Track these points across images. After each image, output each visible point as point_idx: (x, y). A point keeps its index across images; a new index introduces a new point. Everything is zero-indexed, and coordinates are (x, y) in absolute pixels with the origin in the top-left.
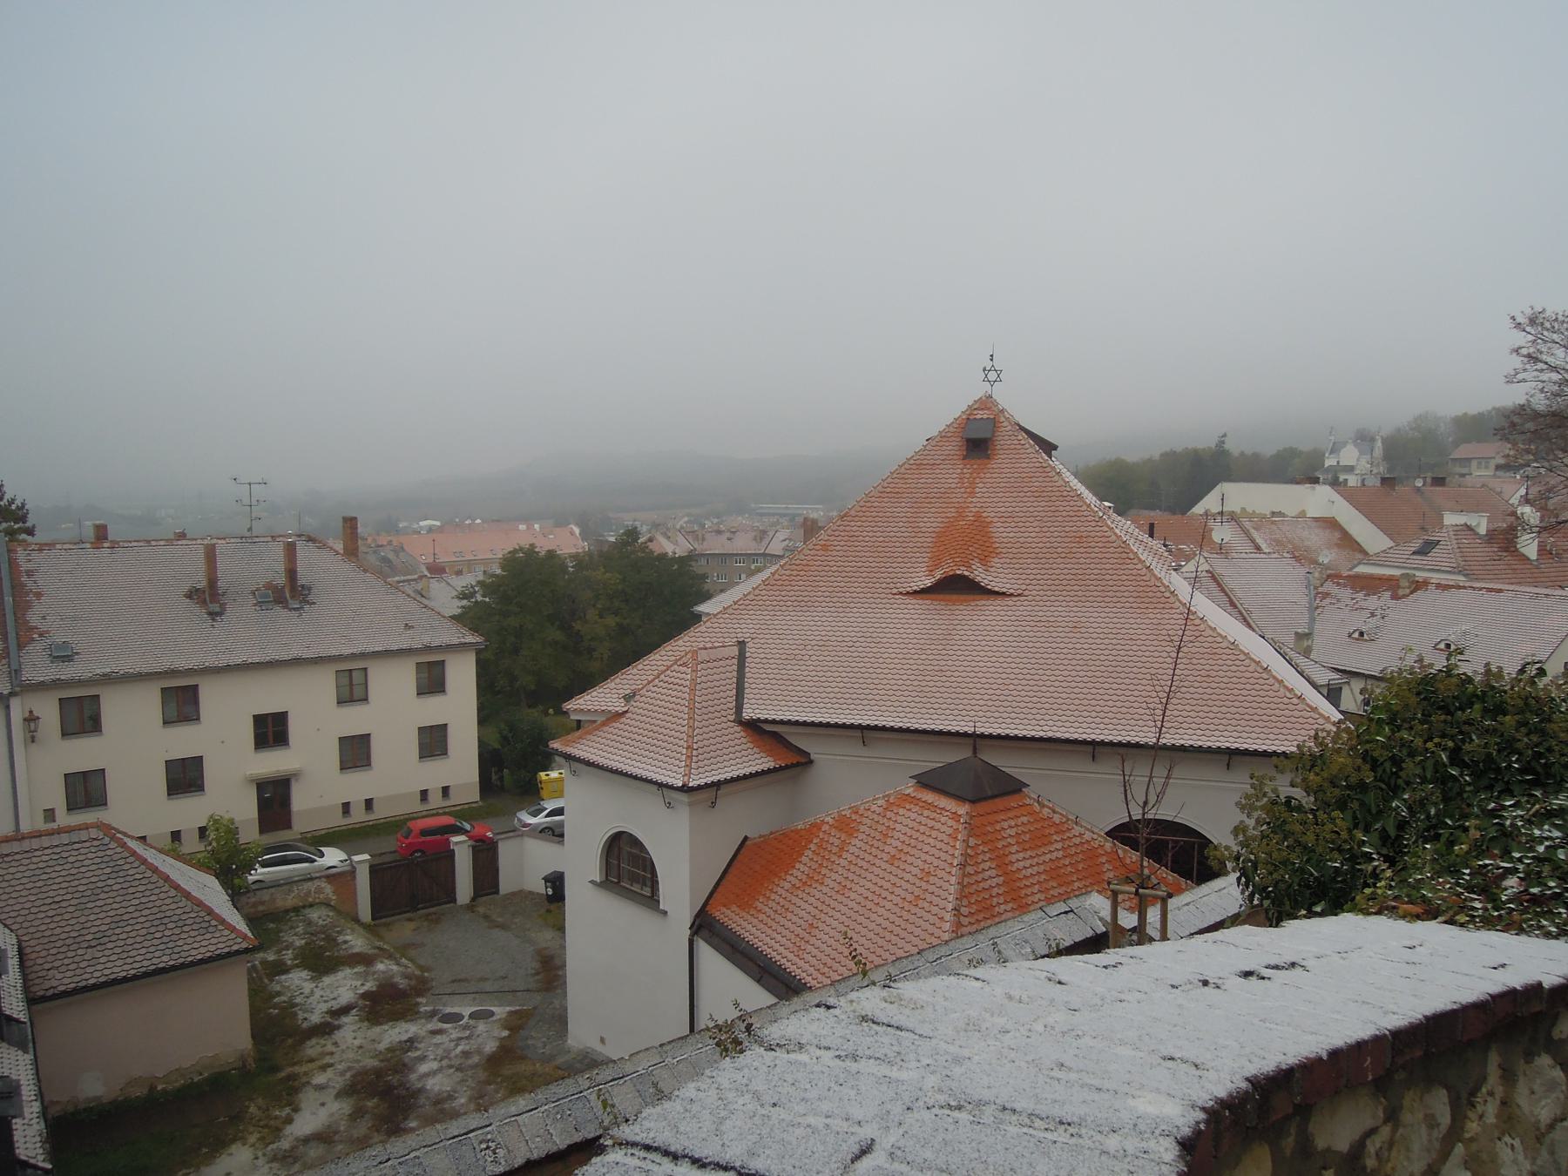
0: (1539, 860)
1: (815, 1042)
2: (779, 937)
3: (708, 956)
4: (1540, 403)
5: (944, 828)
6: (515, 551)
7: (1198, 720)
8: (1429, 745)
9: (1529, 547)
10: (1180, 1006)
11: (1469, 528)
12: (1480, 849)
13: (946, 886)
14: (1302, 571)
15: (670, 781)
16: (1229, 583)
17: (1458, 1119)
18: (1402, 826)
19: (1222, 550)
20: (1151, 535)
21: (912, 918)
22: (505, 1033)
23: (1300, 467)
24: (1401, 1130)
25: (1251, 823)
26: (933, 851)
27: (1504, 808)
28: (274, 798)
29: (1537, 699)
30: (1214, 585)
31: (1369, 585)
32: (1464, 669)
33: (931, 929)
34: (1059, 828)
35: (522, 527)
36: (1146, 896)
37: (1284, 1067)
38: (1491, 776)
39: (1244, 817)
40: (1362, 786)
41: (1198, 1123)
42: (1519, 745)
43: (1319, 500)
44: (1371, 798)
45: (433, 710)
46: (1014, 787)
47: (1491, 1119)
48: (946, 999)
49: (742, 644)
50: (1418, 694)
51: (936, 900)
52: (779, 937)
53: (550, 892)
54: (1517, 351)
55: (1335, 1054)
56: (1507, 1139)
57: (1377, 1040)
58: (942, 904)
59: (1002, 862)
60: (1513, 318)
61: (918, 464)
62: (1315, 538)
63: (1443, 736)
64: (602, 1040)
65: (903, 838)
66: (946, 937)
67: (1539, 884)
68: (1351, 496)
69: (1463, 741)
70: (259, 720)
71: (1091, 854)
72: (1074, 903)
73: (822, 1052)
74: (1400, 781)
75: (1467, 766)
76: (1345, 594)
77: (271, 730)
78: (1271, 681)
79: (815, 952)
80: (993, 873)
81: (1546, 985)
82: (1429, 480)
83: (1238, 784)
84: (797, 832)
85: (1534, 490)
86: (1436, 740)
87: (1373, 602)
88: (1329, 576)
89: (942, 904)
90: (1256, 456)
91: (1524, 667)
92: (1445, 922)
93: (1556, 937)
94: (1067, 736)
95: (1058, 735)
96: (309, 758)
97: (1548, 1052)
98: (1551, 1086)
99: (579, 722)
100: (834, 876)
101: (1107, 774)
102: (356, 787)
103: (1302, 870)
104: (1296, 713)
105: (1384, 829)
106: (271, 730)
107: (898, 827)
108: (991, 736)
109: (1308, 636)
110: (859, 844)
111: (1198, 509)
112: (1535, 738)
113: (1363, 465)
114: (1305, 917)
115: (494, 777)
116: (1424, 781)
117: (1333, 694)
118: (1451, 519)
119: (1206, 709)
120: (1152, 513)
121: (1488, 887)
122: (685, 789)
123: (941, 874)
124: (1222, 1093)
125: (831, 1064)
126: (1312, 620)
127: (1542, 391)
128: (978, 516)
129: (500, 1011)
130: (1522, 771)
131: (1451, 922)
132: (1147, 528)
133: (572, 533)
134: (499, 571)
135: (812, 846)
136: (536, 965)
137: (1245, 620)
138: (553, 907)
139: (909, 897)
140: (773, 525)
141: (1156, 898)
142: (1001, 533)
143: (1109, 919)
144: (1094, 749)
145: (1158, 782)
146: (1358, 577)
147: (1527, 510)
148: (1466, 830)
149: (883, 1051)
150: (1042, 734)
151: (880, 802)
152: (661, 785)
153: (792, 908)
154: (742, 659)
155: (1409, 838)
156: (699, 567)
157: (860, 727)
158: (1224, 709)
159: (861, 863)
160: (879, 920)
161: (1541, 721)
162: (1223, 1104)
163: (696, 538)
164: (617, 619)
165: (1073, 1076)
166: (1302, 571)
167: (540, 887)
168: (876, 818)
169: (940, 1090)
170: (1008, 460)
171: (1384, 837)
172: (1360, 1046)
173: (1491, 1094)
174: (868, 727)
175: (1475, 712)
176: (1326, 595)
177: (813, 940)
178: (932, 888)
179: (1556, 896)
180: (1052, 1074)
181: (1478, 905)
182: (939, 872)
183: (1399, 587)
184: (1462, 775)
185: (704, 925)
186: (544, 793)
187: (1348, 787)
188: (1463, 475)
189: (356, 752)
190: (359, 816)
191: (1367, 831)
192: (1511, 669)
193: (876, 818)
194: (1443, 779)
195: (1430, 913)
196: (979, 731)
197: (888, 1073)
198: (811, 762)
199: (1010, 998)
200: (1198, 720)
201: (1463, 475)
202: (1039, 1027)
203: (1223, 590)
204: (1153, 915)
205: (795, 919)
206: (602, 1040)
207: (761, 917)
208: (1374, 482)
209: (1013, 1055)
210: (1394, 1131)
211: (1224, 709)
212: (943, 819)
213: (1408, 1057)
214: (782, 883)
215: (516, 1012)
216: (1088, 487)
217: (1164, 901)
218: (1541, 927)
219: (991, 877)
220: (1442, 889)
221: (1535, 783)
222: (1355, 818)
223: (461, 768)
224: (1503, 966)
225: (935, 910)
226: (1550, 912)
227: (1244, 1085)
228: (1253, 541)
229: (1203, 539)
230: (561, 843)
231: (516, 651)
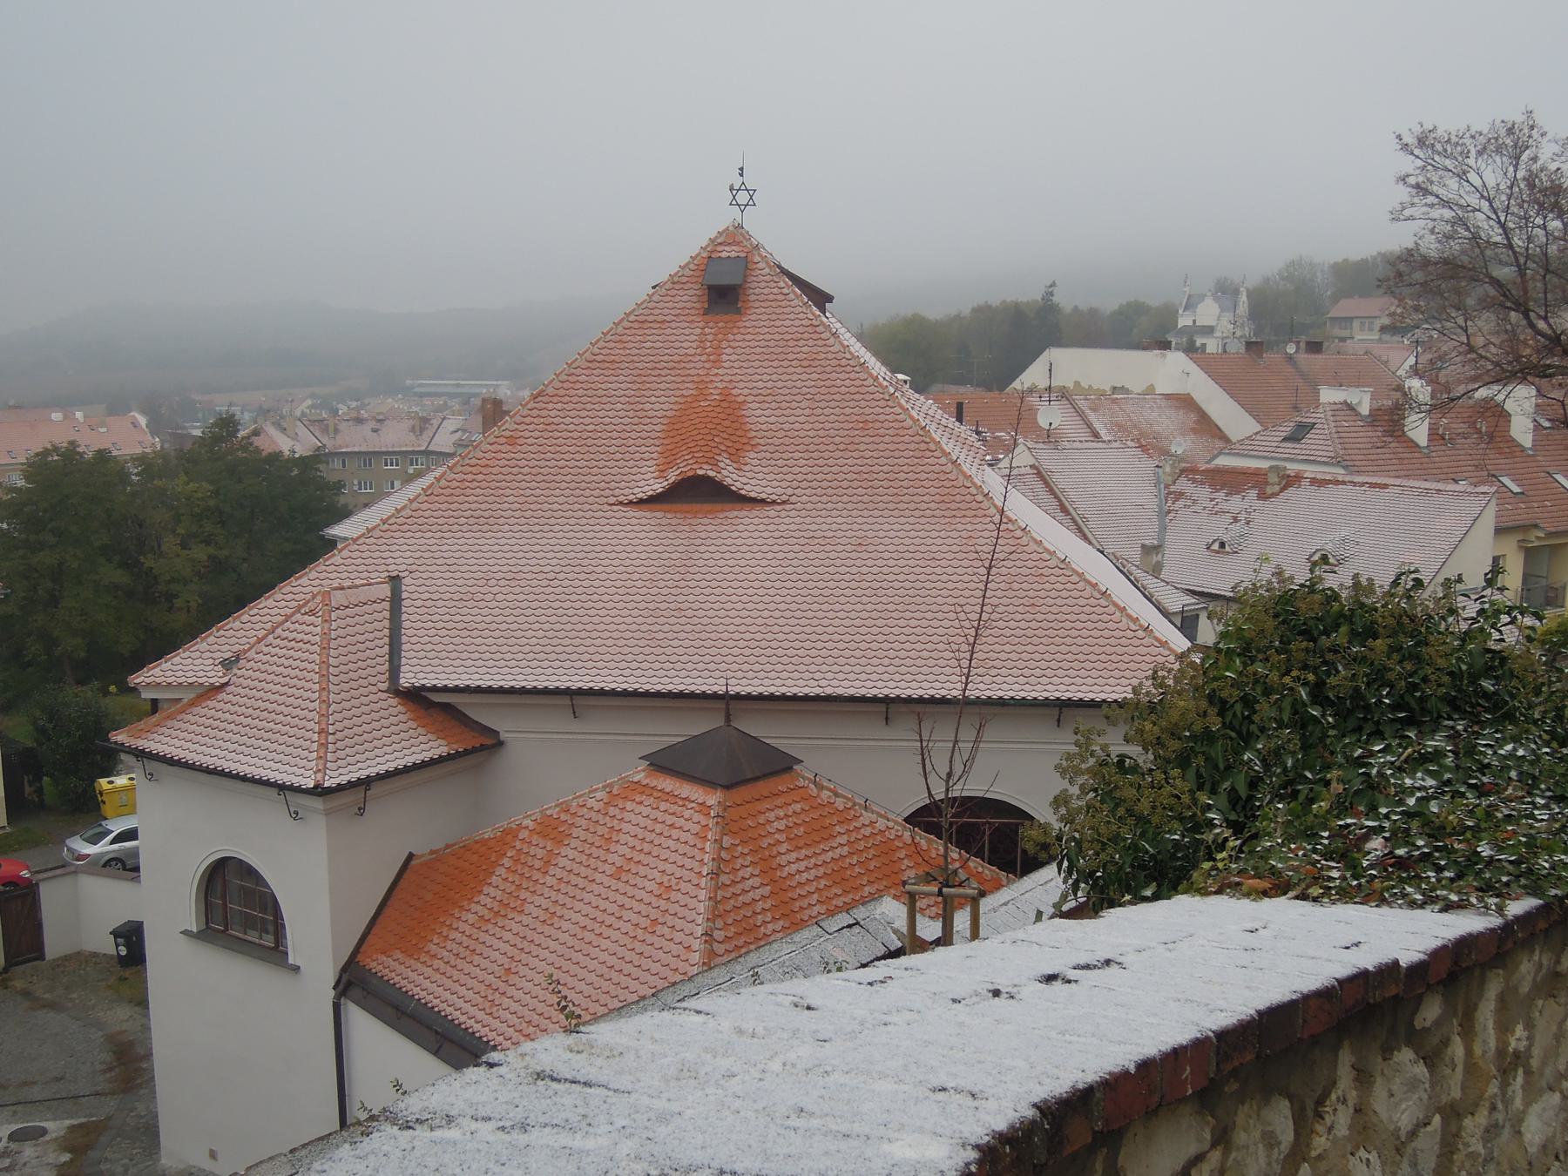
0: (1409, 815)
1: (471, 1112)
2: (462, 991)
3: (364, 1026)
4: (1430, 247)
5: (689, 825)
6: (45, 453)
7: (1020, 664)
8: (1287, 680)
9: (1418, 429)
10: (961, 1024)
11: (1350, 407)
12: (1343, 806)
13: (693, 903)
14: (1152, 463)
15: (296, 781)
16: (1060, 481)
17: (1303, 1131)
18: (1254, 784)
19: (1050, 437)
20: (960, 419)
21: (648, 950)
22: (66, 1157)
23: (1145, 328)
24: (1234, 1155)
25: (1075, 790)
26: (674, 857)
27: (1372, 754)
29: (1412, 619)
30: (1039, 486)
31: (1230, 481)
32: (1331, 581)
33: (674, 963)
34: (846, 817)
35: (57, 416)
36: (953, 896)
37: (1081, 1086)
38: (1358, 716)
39: (1065, 784)
40: (1208, 737)
41: (967, 1165)
42: (1391, 676)
43: (1171, 371)
44: (1217, 751)
46: (783, 765)
47: (1342, 1131)
48: (654, 1040)
49: (395, 581)
50: (1276, 616)
51: (679, 924)
52: (462, 991)
53: (123, 951)
54: (1403, 179)
55: (1145, 1065)
56: (1362, 1153)
57: (1199, 1044)
58: (688, 928)
59: (768, 867)
60: (1399, 137)
61: (641, 321)
62: (1166, 422)
63: (1305, 667)
64: (213, 1155)
65: (632, 842)
66: (695, 970)
67: (1407, 844)
68: (1213, 367)
69: (1328, 673)
71: (886, 849)
72: (860, 913)
73: (479, 1125)
74: (1253, 728)
75: (1331, 704)
76: (1203, 493)
78: (1112, 609)
79: (515, 1007)
80: (756, 881)
81: (1403, 964)
82: (1302, 345)
83: (1063, 742)
84: (484, 842)
85: (1424, 359)
86: (1295, 673)
87: (1236, 503)
88: (1183, 471)
89: (688, 928)
90: (1093, 312)
91: (1398, 577)
92: (1297, 898)
93: (1422, 906)
94: (851, 692)
95: (840, 691)
97: (1409, 1044)
98: (1413, 1084)
99: (155, 702)
100: (538, 900)
101: (902, 737)
103: (1134, 847)
104: (1143, 650)
105: (1233, 789)
107: (626, 827)
108: (749, 697)
109: (1157, 549)
110: (572, 854)
111: (1016, 384)
112: (1409, 666)
113: (1225, 326)
114: (1131, 903)
115: (28, 789)
116: (1281, 725)
117: (1187, 624)
118: (1329, 395)
119: (1030, 648)
120: (962, 389)
121: (1347, 852)
122: (319, 791)
123: (684, 887)
124: (1001, 1125)
125: (491, 1138)
126: (1163, 528)
127: (1432, 231)
128: (726, 395)
129: (55, 1127)
130: (1395, 707)
131: (1303, 897)
132: (954, 410)
133: (135, 425)
134: (21, 483)
135: (506, 862)
136: (108, 1057)
137: (1080, 530)
138: (127, 973)
139: (644, 922)
140: (438, 410)
141: (965, 897)
142: (758, 416)
143: (904, 930)
144: (887, 708)
145: (965, 746)
146: (1219, 471)
147: (1415, 384)
148: (1327, 783)
149: (563, 1115)
150: (818, 691)
151: (599, 795)
152: (282, 788)
153: (480, 948)
154: (396, 601)
155: (1263, 796)
156: (331, 471)
157: (568, 692)
158: (1053, 649)
159: (575, 880)
160: (604, 956)
161: (1417, 644)
162: (1002, 1138)
163: (326, 430)
164: (211, 550)
165: (815, 1123)
166: (1152, 463)
167: (107, 946)
168: (594, 816)
169: (638, 1158)
170: (770, 313)
171: (1234, 799)
172: (1176, 1056)
173: (1344, 1101)
174: (580, 692)
175: (1340, 637)
176: (1180, 495)
177: (511, 991)
178: (673, 908)
179: (1425, 857)
180: (789, 1122)
181: (1335, 874)
182: (683, 885)
183: (1267, 483)
184: (1323, 716)
185: (355, 982)
186: (107, 809)
187: (1193, 737)
188: (1343, 340)
191: (1213, 792)
192: (1383, 580)
193: (594, 816)
194: (1301, 722)
195: (1279, 888)
196: (733, 690)
197: (570, 1144)
198: (501, 744)
199: (740, 1032)
200: (1020, 664)
201: (1343, 340)
202: (776, 1066)
203: (1052, 491)
204: (961, 920)
205: (485, 963)
206: (213, 1155)
207: (436, 963)
208: (1237, 347)
209: (737, 1104)
210: (1226, 1154)
211: (1053, 649)
212: (687, 814)
213: (1236, 1063)
214: (465, 915)
215: (81, 1126)
216: (876, 354)
217: (974, 901)
218: (1404, 896)
219: (754, 888)
220: (1290, 858)
221: (1410, 722)
222: (1199, 776)
224: (1357, 945)
225: (678, 936)
226: (1418, 876)
227: (1030, 1113)
228: (1089, 426)
229: (1022, 420)
230: (137, 879)
231: (54, 601)
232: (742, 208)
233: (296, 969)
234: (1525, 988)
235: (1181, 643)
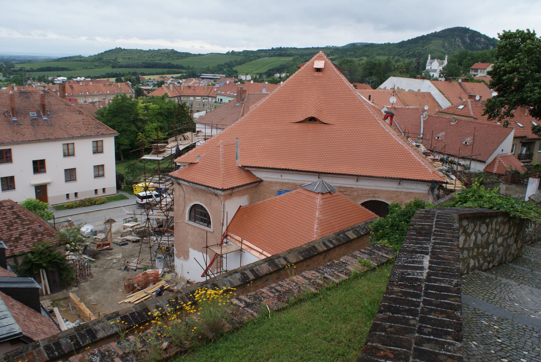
20: (369, 99)
28: (41, 190)
45: (99, 159)
70: (35, 163)
77: (39, 166)
96: (53, 177)
98: (485, 228)
102: (71, 188)
106: (39, 166)
189: (70, 175)
190: (72, 199)
223: (109, 182)
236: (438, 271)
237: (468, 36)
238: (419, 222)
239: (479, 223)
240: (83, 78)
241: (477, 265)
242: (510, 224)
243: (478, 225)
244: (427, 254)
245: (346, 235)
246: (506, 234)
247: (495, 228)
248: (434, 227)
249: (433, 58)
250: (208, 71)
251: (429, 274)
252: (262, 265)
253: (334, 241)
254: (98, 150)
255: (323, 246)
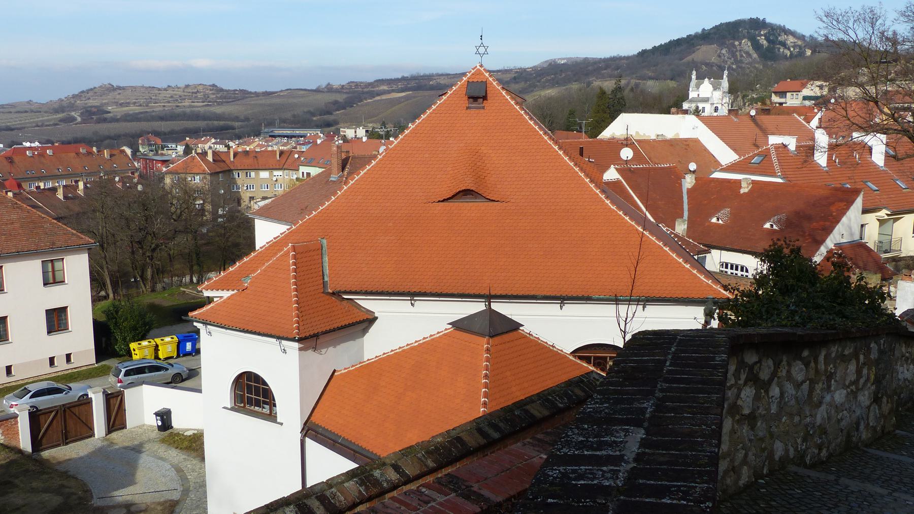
11: (785, 146)
53: (160, 423)
68: (710, 122)
98: (801, 370)
185: (310, 430)
223: (80, 341)
232: (481, 55)
233: (282, 424)
234: (833, 355)
235: (25, 442)
236: (661, 464)
237: (765, 35)
238: (636, 355)
239: (785, 358)
240: (37, 144)
241: (792, 453)
242: (858, 360)
243: (784, 363)
244: (638, 424)
245: (527, 411)
246: (852, 383)
247: (826, 370)
248: (668, 364)
249: (700, 78)
250: (284, 123)
251: (633, 474)
252: (346, 485)
253: (501, 424)
254: (51, 279)
255: (477, 435)
